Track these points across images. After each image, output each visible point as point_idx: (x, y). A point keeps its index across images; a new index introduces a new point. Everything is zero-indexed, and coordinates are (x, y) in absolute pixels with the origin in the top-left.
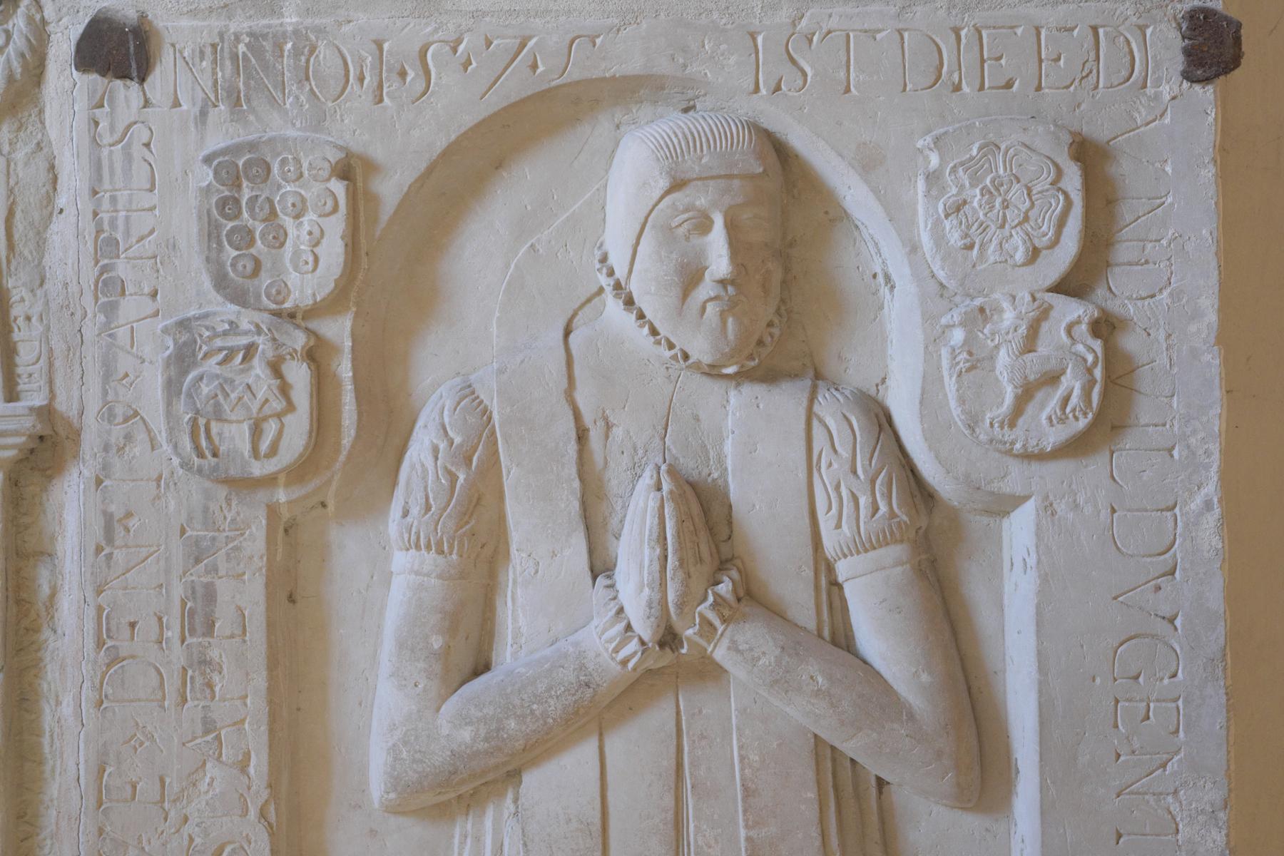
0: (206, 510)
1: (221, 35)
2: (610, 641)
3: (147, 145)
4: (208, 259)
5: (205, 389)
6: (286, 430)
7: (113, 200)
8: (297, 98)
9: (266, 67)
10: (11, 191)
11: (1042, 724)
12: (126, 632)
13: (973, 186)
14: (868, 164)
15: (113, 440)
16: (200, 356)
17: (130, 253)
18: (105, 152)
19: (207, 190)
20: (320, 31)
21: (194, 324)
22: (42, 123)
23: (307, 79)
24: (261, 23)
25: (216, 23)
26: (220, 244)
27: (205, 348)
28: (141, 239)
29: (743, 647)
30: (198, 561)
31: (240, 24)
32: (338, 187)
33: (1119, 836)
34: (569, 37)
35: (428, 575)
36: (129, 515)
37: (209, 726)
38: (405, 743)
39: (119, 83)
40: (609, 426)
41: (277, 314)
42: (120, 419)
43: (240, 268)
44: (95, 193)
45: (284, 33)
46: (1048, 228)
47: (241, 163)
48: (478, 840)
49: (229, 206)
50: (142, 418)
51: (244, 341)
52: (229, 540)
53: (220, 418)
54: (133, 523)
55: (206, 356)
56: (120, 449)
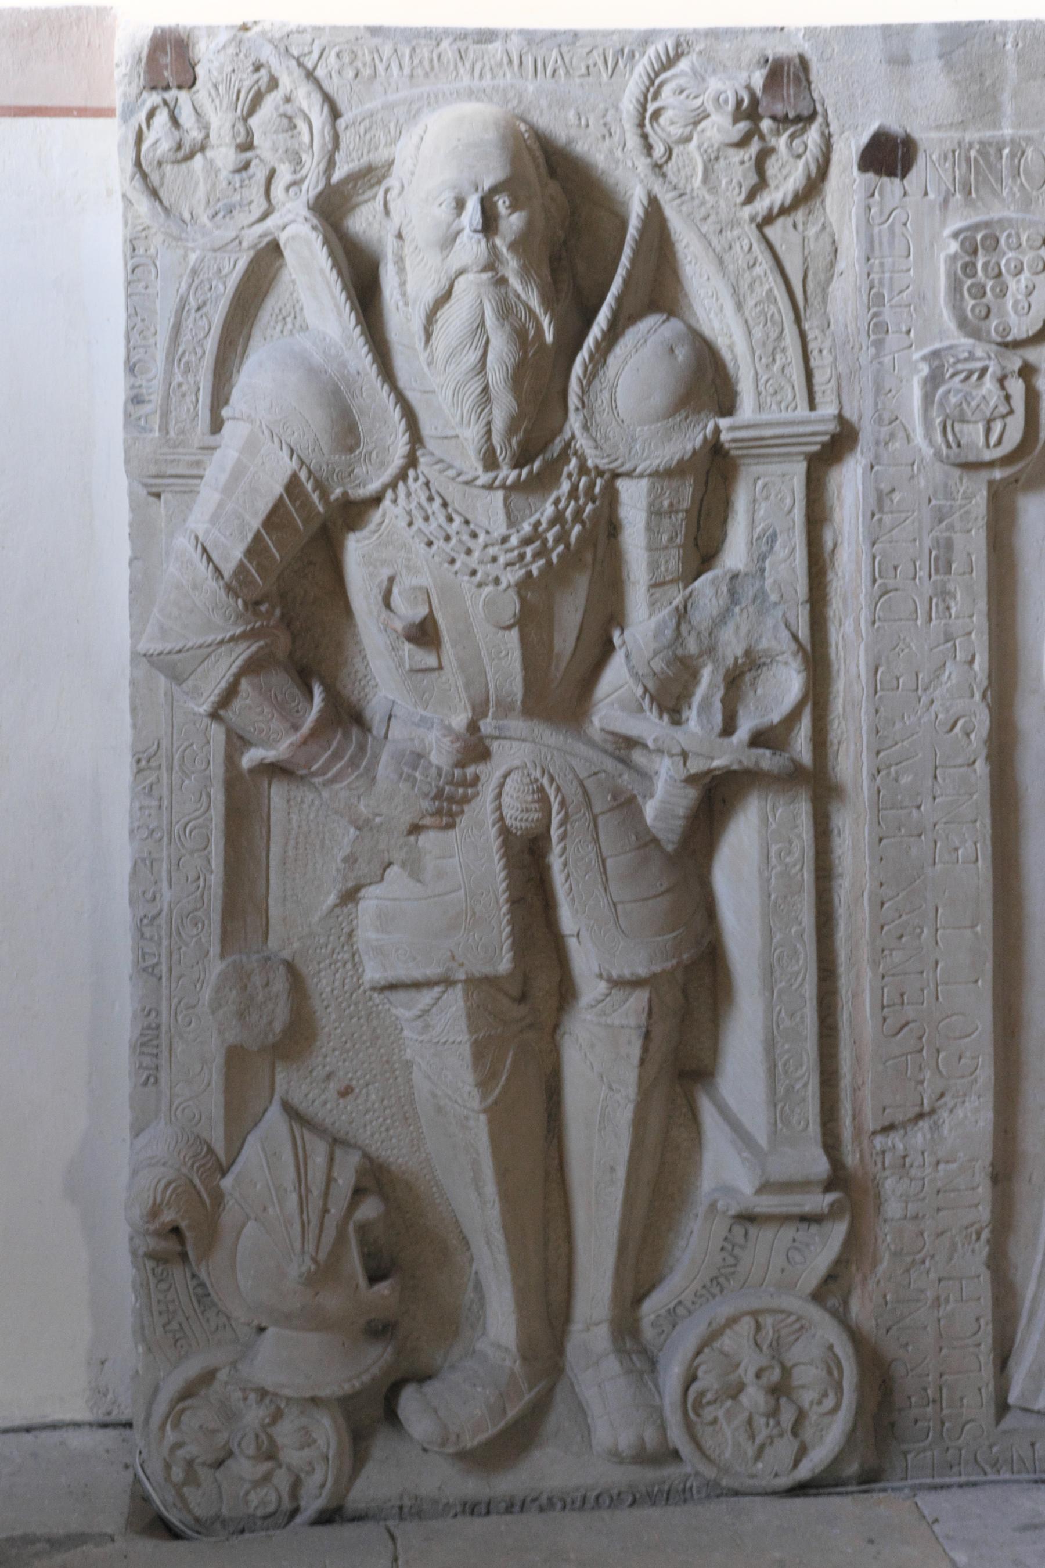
0: (946, 485)
1: (960, 144)
3: (905, 224)
4: (954, 307)
5: (953, 400)
6: (1007, 428)
7: (882, 265)
8: (1011, 189)
9: (990, 166)
10: (805, 259)
12: (892, 573)
15: (882, 437)
16: (948, 376)
17: (894, 302)
18: (876, 229)
19: (954, 258)
20: (1029, 140)
21: (943, 353)
22: (824, 209)
23: (1019, 174)
24: (988, 134)
25: (956, 135)
27: (951, 371)
28: (901, 292)
30: (941, 521)
31: (973, 135)
36: (893, 490)
37: (949, 638)
39: (885, 179)
42: (886, 422)
43: (977, 311)
44: (868, 259)
45: (1004, 142)
47: (979, 238)
49: (969, 269)
50: (901, 423)
51: (979, 365)
53: (963, 420)
54: (897, 497)
55: (953, 375)
56: (886, 444)
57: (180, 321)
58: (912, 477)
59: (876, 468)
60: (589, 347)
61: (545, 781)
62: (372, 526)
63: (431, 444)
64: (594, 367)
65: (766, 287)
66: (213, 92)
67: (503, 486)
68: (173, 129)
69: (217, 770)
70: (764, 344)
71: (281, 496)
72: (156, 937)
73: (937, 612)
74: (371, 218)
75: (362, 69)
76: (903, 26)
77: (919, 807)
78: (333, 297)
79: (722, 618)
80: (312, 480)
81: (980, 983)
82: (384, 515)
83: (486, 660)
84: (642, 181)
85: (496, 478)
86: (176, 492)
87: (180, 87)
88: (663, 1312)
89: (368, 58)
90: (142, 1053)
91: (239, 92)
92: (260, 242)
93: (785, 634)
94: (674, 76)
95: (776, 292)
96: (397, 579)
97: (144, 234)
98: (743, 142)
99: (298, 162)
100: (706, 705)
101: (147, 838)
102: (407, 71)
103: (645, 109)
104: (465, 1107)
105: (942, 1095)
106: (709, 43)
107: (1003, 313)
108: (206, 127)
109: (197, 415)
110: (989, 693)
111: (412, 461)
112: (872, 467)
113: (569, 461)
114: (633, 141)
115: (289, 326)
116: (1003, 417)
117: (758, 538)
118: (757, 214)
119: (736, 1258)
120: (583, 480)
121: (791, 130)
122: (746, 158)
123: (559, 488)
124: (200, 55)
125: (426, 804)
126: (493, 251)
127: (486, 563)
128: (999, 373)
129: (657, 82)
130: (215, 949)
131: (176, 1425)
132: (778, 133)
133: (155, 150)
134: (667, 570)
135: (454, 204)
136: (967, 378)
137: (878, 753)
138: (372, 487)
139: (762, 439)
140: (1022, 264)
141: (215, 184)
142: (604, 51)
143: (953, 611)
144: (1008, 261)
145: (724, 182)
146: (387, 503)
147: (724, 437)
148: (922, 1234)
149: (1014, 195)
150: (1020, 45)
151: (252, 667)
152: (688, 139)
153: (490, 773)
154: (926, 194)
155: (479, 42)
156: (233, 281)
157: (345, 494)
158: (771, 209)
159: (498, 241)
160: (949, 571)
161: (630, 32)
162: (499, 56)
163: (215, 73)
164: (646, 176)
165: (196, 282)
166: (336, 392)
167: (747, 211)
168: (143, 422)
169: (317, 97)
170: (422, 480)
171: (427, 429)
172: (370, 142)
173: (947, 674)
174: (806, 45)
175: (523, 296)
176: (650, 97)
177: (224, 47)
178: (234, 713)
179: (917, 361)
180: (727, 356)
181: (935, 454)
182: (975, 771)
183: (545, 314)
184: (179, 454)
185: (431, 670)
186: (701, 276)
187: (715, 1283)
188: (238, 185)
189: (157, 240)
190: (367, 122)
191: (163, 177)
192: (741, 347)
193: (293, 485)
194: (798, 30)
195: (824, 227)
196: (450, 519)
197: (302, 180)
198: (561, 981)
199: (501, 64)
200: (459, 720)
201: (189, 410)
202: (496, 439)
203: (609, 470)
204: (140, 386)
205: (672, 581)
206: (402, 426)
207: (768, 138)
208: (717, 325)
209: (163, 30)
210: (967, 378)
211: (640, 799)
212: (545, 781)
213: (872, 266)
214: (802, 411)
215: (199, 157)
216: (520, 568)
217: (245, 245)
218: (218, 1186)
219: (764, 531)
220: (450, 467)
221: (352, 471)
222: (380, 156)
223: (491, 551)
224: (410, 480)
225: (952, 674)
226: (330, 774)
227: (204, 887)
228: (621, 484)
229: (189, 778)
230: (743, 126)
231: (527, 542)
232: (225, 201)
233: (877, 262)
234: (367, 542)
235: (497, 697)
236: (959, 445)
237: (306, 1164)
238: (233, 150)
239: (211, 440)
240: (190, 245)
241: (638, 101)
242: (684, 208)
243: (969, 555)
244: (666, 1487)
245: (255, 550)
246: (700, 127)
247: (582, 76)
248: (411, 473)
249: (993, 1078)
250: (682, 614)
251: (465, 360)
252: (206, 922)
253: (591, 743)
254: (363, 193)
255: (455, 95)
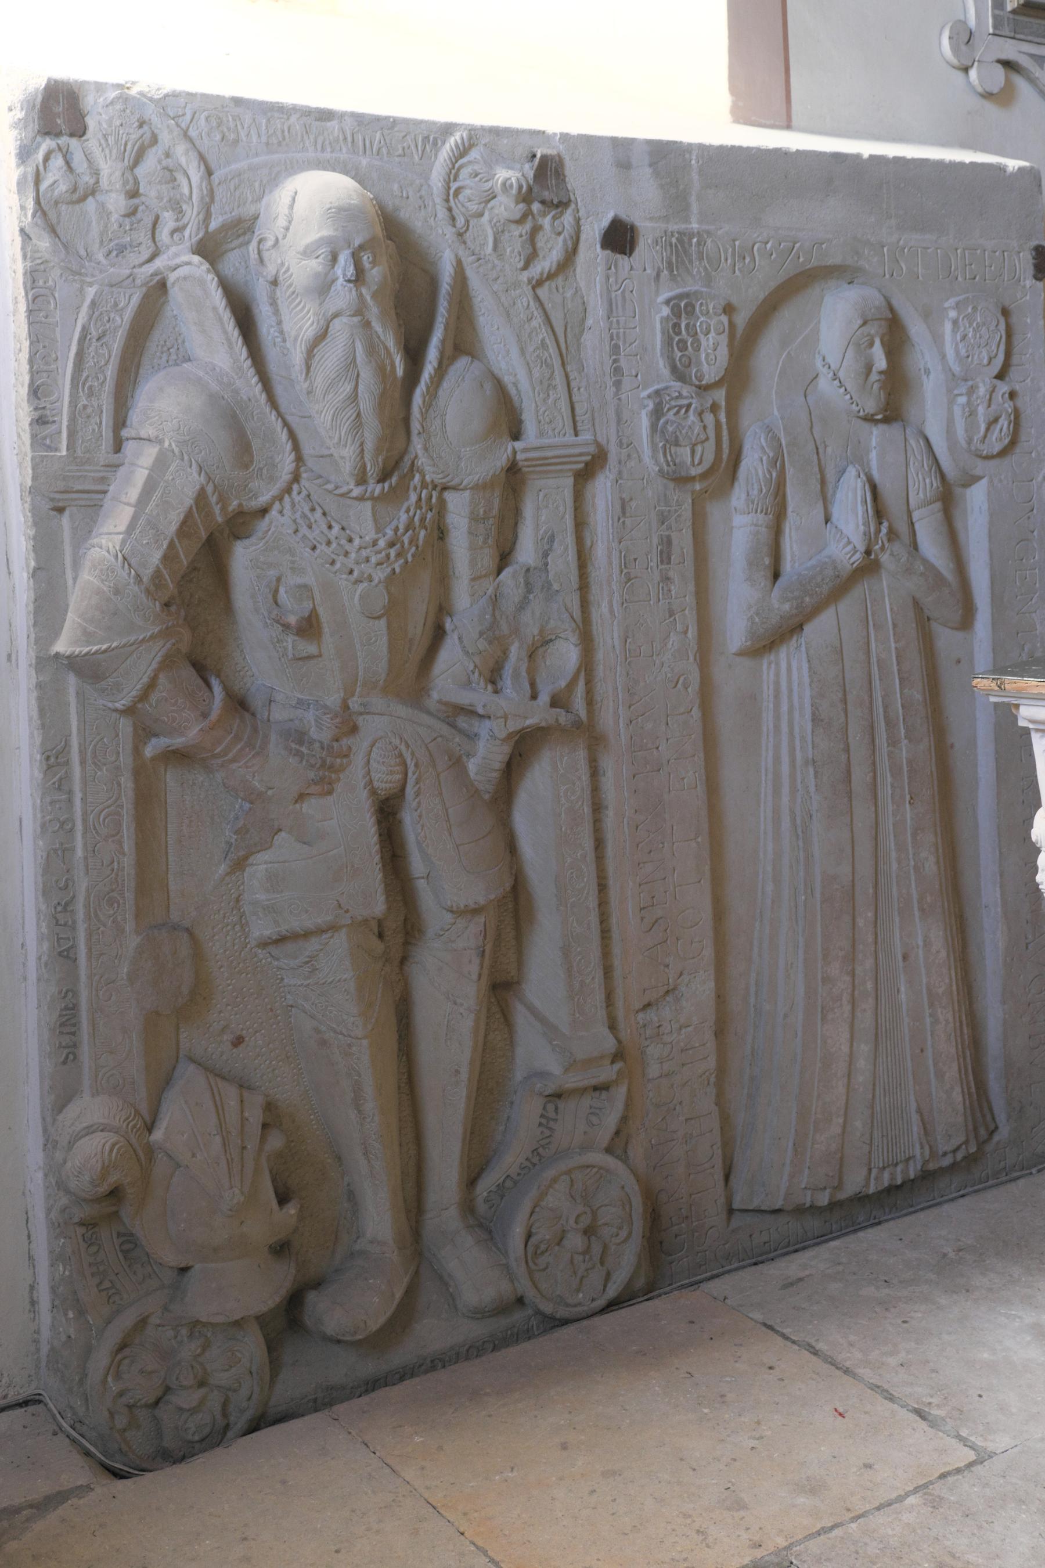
0: (665, 495)
1: (665, 232)
2: (847, 554)
3: (632, 292)
7: (618, 322)
9: (685, 251)
11: (992, 583)
13: (970, 327)
14: (927, 315)
16: (665, 410)
20: (708, 233)
24: (683, 226)
25: (663, 226)
26: (672, 348)
27: (667, 406)
28: (631, 344)
29: (895, 553)
30: (663, 523)
31: (673, 227)
32: (724, 319)
33: (1018, 633)
34: (813, 243)
35: (761, 526)
36: (631, 499)
38: (757, 614)
39: (619, 256)
40: (826, 447)
41: (699, 387)
45: (693, 233)
46: (994, 348)
47: (682, 305)
48: (778, 665)
51: (685, 402)
52: (676, 511)
53: (677, 444)
54: (633, 504)
57: (83, 350)
58: (643, 489)
59: (619, 482)
60: (426, 381)
61: (403, 747)
62: (260, 534)
63: (310, 462)
64: (430, 398)
65: (541, 337)
66: (103, 142)
67: (372, 498)
68: (68, 173)
69: (126, 760)
70: (541, 382)
71: (191, 508)
72: (70, 923)
73: (663, 594)
74: (237, 265)
75: (227, 134)
76: (626, 139)
77: (657, 748)
78: (225, 332)
79: (522, 605)
80: (216, 493)
81: (702, 881)
82: (271, 523)
83: (358, 646)
84: (450, 246)
85: (366, 491)
86: (81, 506)
87: (72, 135)
88: (493, 1188)
89: (232, 124)
90: (61, 1033)
91: (126, 144)
92: (151, 280)
93: (566, 616)
94: (470, 162)
95: (548, 341)
96: (283, 579)
97: (42, 267)
98: (519, 222)
99: (180, 212)
100: (516, 675)
101: (58, 831)
102: (264, 139)
103: (449, 188)
104: (350, 1036)
105: (681, 974)
106: (492, 138)
107: (699, 363)
108: (96, 173)
109: (102, 436)
110: (698, 655)
111: (296, 478)
112: (617, 482)
113: (413, 477)
114: (442, 213)
115: (174, 357)
116: (702, 442)
117: (542, 539)
118: (533, 278)
119: (550, 1129)
120: (424, 492)
121: (553, 212)
122: (524, 232)
123: (407, 500)
124: (89, 108)
125: (312, 775)
126: (360, 296)
127: (361, 563)
128: (699, 409)
129: (457, 165)
130: (129, 926)
131: (118, 1376)
132: (544, 215)
133: (53, 191)
134: (482, 567)
135: (330, 257)
136: (678, 412)
137: (630, 707)
138: (263, 499)
139: (546, 458)
140: (710, 325)
141: (106, 227)
142: (415, 135)
143: (673, 593)
144: (701, 323)
145: (508, 250)
146: (274, 513)
147: (520, 457)
148: (672, 1085)
149: (701, 273)
150: (700, 162)
151: (167, 663)
152: (481, 215)
153: (360, 744)
154: (645, 270)
155: (320, 119)
156: (128, 315)
157: (240, 505)
158: (542, 274)
159: (364, 291)
160: (669, 563)
161: (434, 123)
162: (336, 134)
163: (105, 126)
164: (453, 242)
165: (97, 314)
166: (234, 416)
167: (525, 276)
168: (48, 442)
169: (193, 155)
170: (304, 493)
171: (307, 450)
172: (239, 198)
173: (671, 643)
174: (561, 147)
175: (382, 338)
176: (452, 178)
177: (112, 103)
178: (151, 706)
179: (643, 398)
180: (513, 391)
181: (659, 471)
182: (692, 716)
183: (398, 353)
184: (86, 471)
185: (310, 657)
186: (492, 326)
187: (535, 1153)
188: (128, 228)
189: (56, 273)
190: (236, 180)
191: (59, 215)
192: (524, 384)
193: (201, 497)
194: (555, 134)
195: (577, 291)
196: (330, 527)
197: (184, 227)
198: (405, 920)
199: (337, 140)
200: (333, 700)
201: (93, 430)
202: (367, 457)
203: (441, 483)
204: (44, 408)
205: (485, 576)
206: (289, 446)
207: (537, 217)
208: (503, 365)
209: (56, 81)
210: (678, 412)
211: (464, 758)
212: (403, 747)
213: (611, 322)
214: (570, 438)
215: (90, 198)
216: (387, 567)
217: (138, 282)
218: (148, 1143)
219: (546, 532)
220: (328, 482)
221: (246, 486)
222: (250, 210)
223: (364, 553)
224: (295, 493)
225: (674, 640)
226: (230, 756)
227: (118, 870)
228: (448, 496)
229: (101, 770)
230: (522, 206)
231: (391, 545)
232: (116, 242)
233: (615, 320)
234: (254, 548)
235: (364, 678)
236: (675, 465)
237: (223, 1109)
238: (122, 197)
239: (114, 458)
240: (88, 279)
241: (444, 180)
242: (481, 270)
243: (682, 548)
244: (516, 1330)
245: (169, 557)
246: (489, 205)
247: (399, 156)
248: (295, 487)
249: (713, 955)
250: (495, 600)
251: (342, 390)
252: (121, 902)
253: (429, 713)
254: (231, 241)
255: (306, 163)
